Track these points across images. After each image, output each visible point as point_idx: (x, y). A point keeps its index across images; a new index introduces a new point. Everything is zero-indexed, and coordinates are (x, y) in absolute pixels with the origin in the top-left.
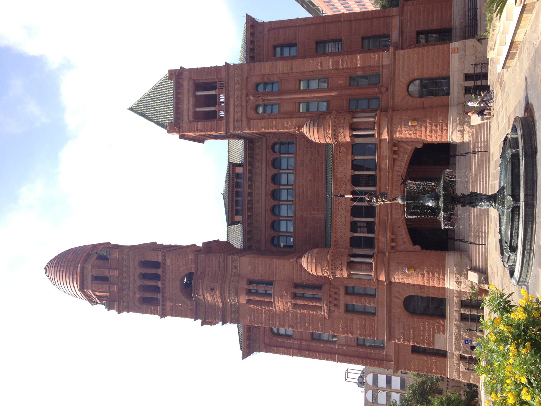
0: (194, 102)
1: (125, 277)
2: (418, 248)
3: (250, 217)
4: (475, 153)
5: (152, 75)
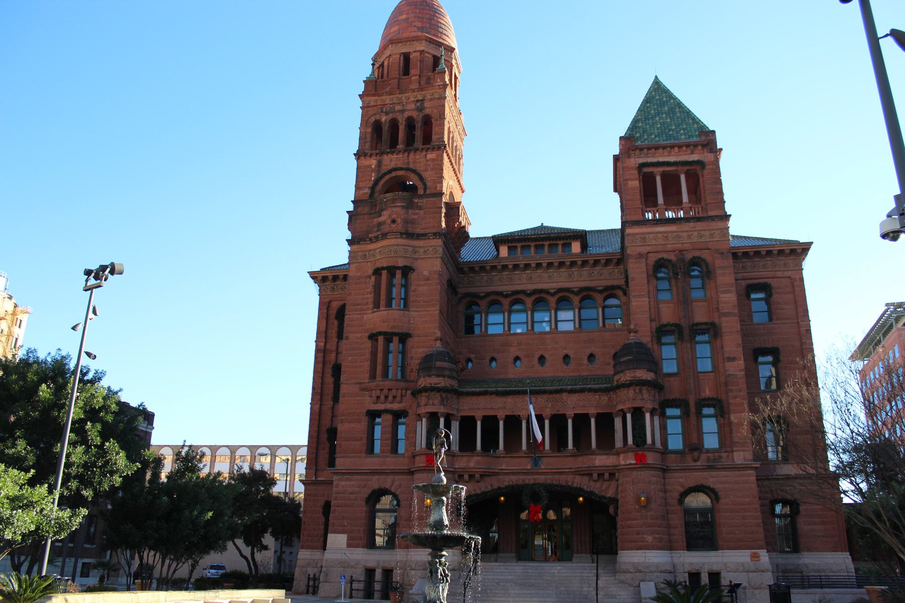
1: (404, 125)
3: (505, 267)
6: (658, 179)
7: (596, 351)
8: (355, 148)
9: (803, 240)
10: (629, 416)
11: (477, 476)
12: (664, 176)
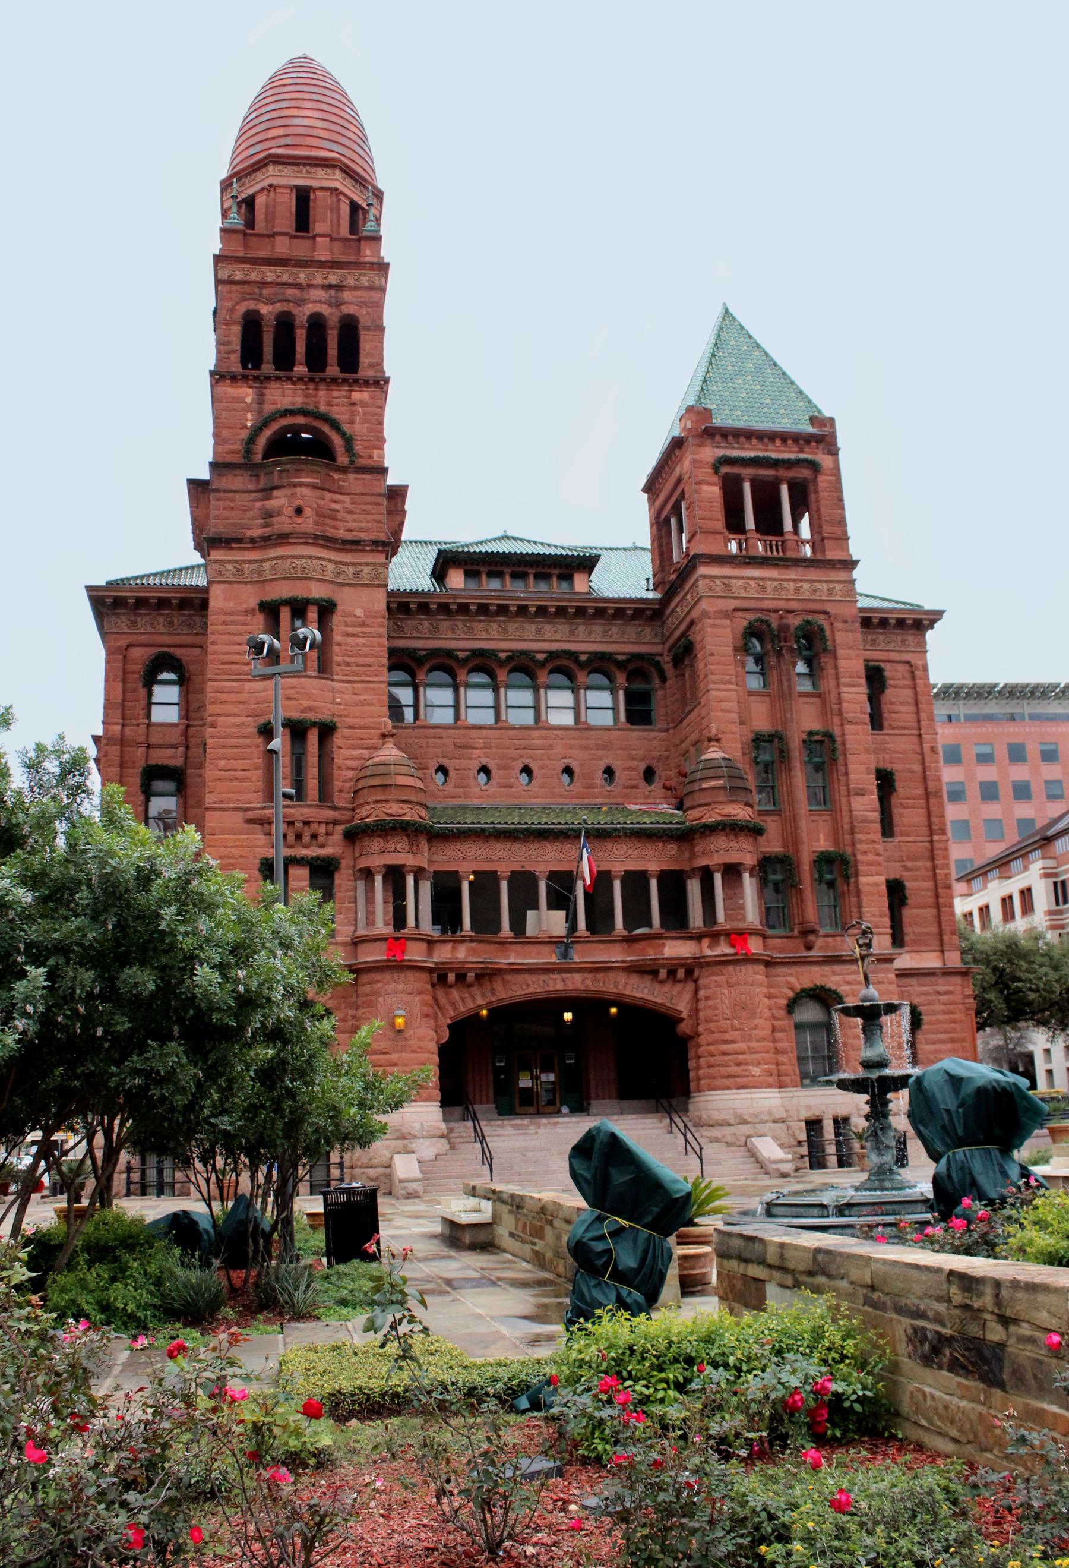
0: (755, 479)
2: (446, 1035)
5: (828, 372)
6: (747, 487)
7: (617, 765)
8: (211, 363)
9: (929, 605)
11: (471, 976)
12: (755, 484)
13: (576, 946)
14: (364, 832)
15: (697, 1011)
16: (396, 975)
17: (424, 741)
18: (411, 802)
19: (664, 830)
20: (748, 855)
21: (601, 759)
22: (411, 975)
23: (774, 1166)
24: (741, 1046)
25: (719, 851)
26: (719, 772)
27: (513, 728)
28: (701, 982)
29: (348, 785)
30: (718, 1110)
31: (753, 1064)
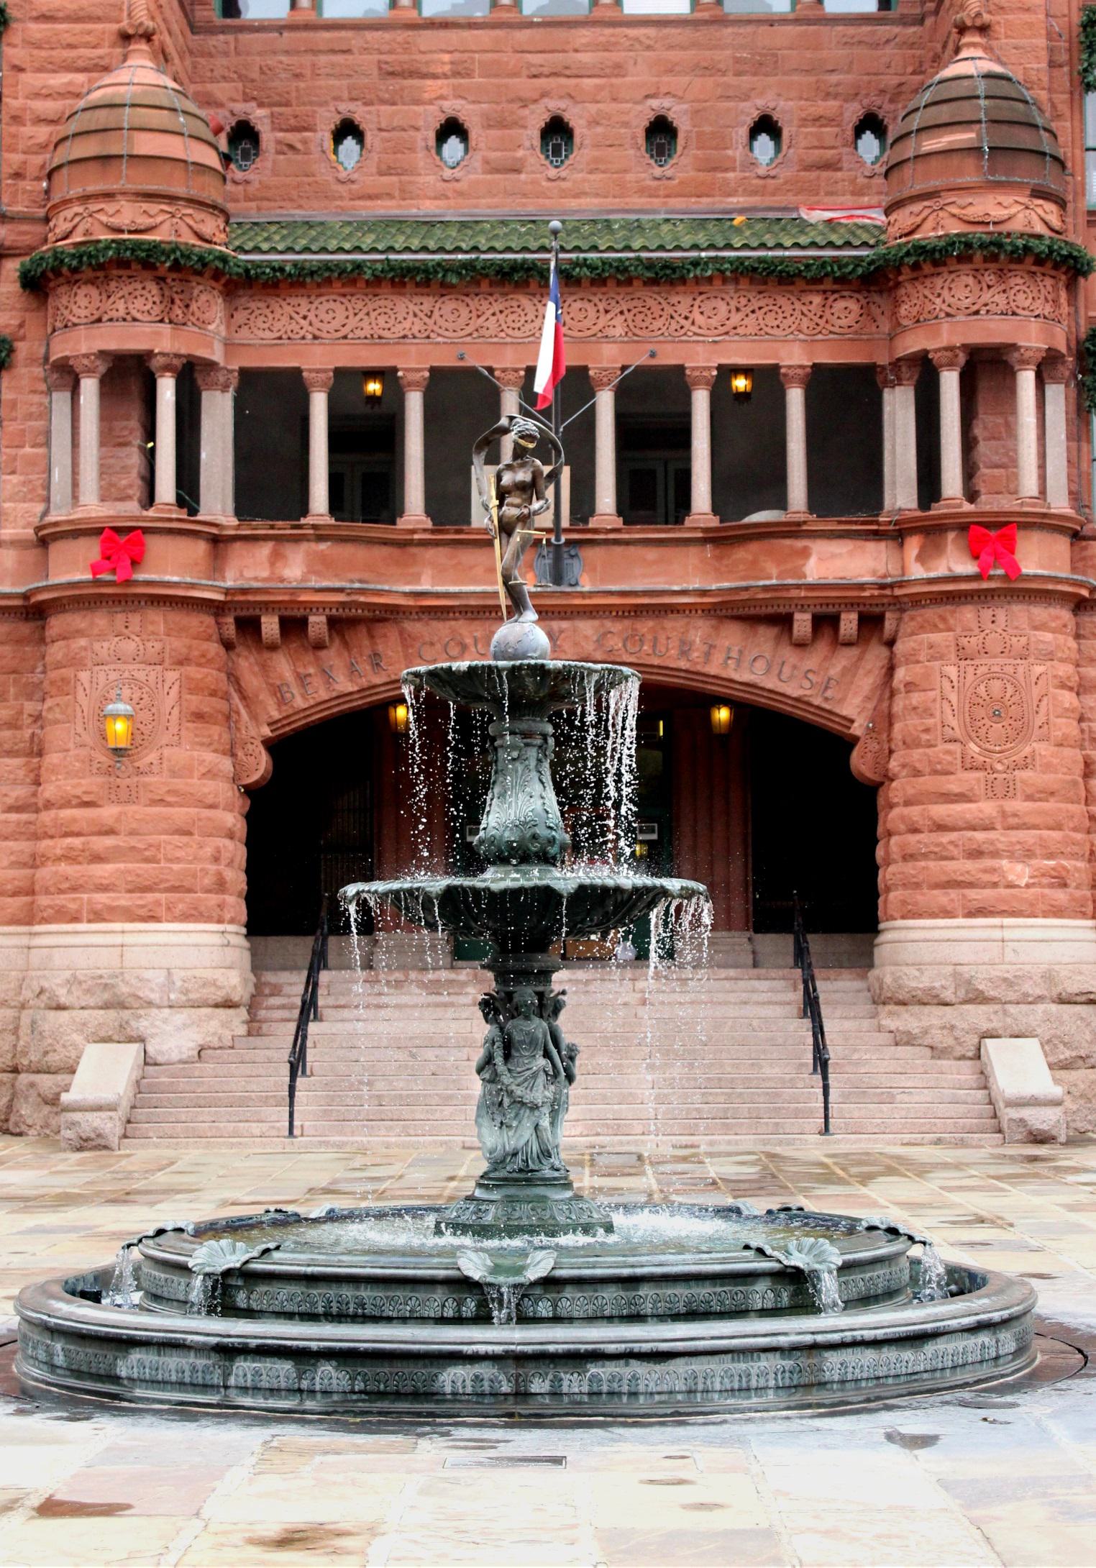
2: (259, 765)
4: (811, 1007)
10: (950, 383)
11: (317, 623)
13: (589, 553)
14: (57, 272)
15: (890, 719)
16: (120, 618)
17: (307, 59)
18: (171, 199)
19: (823, 263)
20: (1034, 326)
21: (746, 98)
22: (158, 619)
23: (1014, 1113)
24: (986, 808)
25: (955, 315)
26: (964, 111)
27: (530, 25)
28: (900, 647)
29: (38, 160)
30: (918, 965)
31: (1011, 856)
